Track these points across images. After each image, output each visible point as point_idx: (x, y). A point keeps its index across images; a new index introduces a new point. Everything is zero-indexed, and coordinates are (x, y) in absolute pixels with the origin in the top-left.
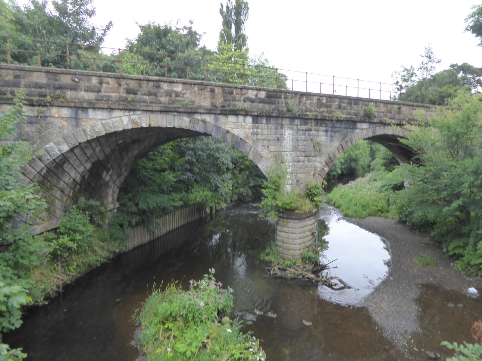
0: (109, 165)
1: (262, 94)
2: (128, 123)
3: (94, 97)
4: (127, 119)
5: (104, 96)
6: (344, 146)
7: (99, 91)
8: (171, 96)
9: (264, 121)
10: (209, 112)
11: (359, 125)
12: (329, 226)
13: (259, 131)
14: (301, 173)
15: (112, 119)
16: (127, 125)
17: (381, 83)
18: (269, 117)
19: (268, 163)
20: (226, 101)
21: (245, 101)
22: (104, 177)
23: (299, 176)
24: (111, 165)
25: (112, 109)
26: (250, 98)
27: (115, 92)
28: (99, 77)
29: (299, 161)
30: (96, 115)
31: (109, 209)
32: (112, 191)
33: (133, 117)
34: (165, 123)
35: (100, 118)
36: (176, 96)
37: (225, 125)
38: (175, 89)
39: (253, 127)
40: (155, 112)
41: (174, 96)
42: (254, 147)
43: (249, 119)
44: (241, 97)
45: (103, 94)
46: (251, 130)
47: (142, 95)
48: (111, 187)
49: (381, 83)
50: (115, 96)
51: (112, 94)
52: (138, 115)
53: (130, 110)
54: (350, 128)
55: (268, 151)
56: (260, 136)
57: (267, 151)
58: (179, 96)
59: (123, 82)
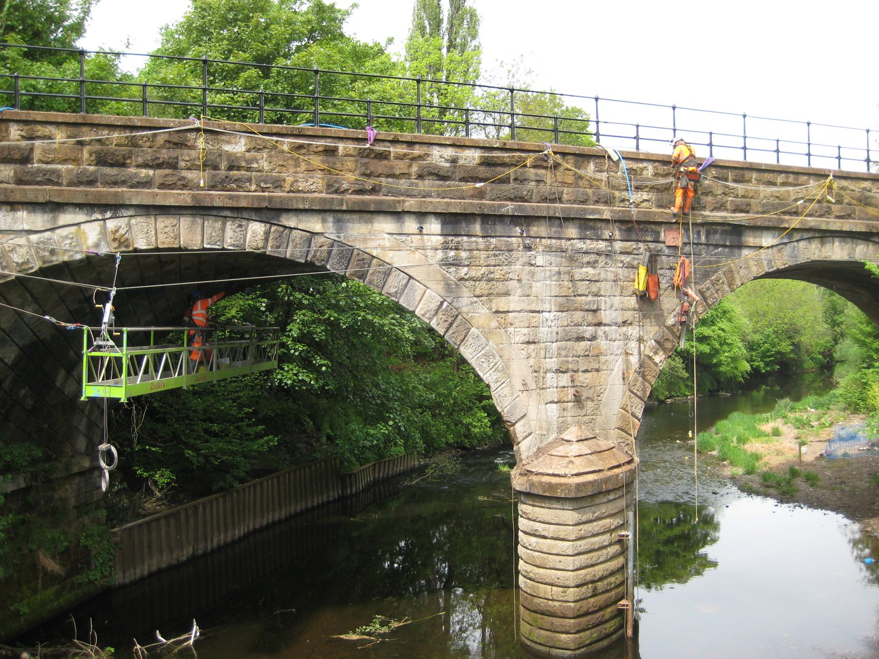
0: (72, 353)
1: (472, 157)
2: (100, 240)
3: (12, 174)
4: (99, 229)
5: (39, 170)
6: (708, 294)
7: (26, 160)
8: (216, 168)
9: (477, 228)
10: (322, 211)
11: (750, 239)
12: (718, 518)
13: (464, 254)
14: (586, 371)
15: (58, 231)
16: (97, 245)
17: (809, 124)
18: (489, 219)
19: (491, 343)
20: (369, 176)
21: (420, 177)
22: (58, 384)
23: (581, 379)
24: (75, 352)
25: (55, 207)
26: (436, 167)
27: (65, 161)
28: (26, 122)
29: (580, 339)
30: (15, 221)
31: (76, 470)
32: (85, 420)
33: (111, 225)
34: (199, 238)
35: (26, 227)
36: (231, 168)
37: (365, 240)
38: (227, 148)
39: (445, 247)
40: (173, 211)
41: (223, 165)
42: (449, 300)
43: (434, 226)
44: (410, 166)
45: (36, 165)
46: (440, 254)
47: (138, 166)
48: (83, 411)
49: (809, 124)
50: (69, 171)
51: (60, 166)
52: (126, 219)
53: (103, 207)
54: (724, 246)
55: (490, 309)
56: (466, 269)
57: (485, 310)
58: (239, 168)
59: (88, 135)
